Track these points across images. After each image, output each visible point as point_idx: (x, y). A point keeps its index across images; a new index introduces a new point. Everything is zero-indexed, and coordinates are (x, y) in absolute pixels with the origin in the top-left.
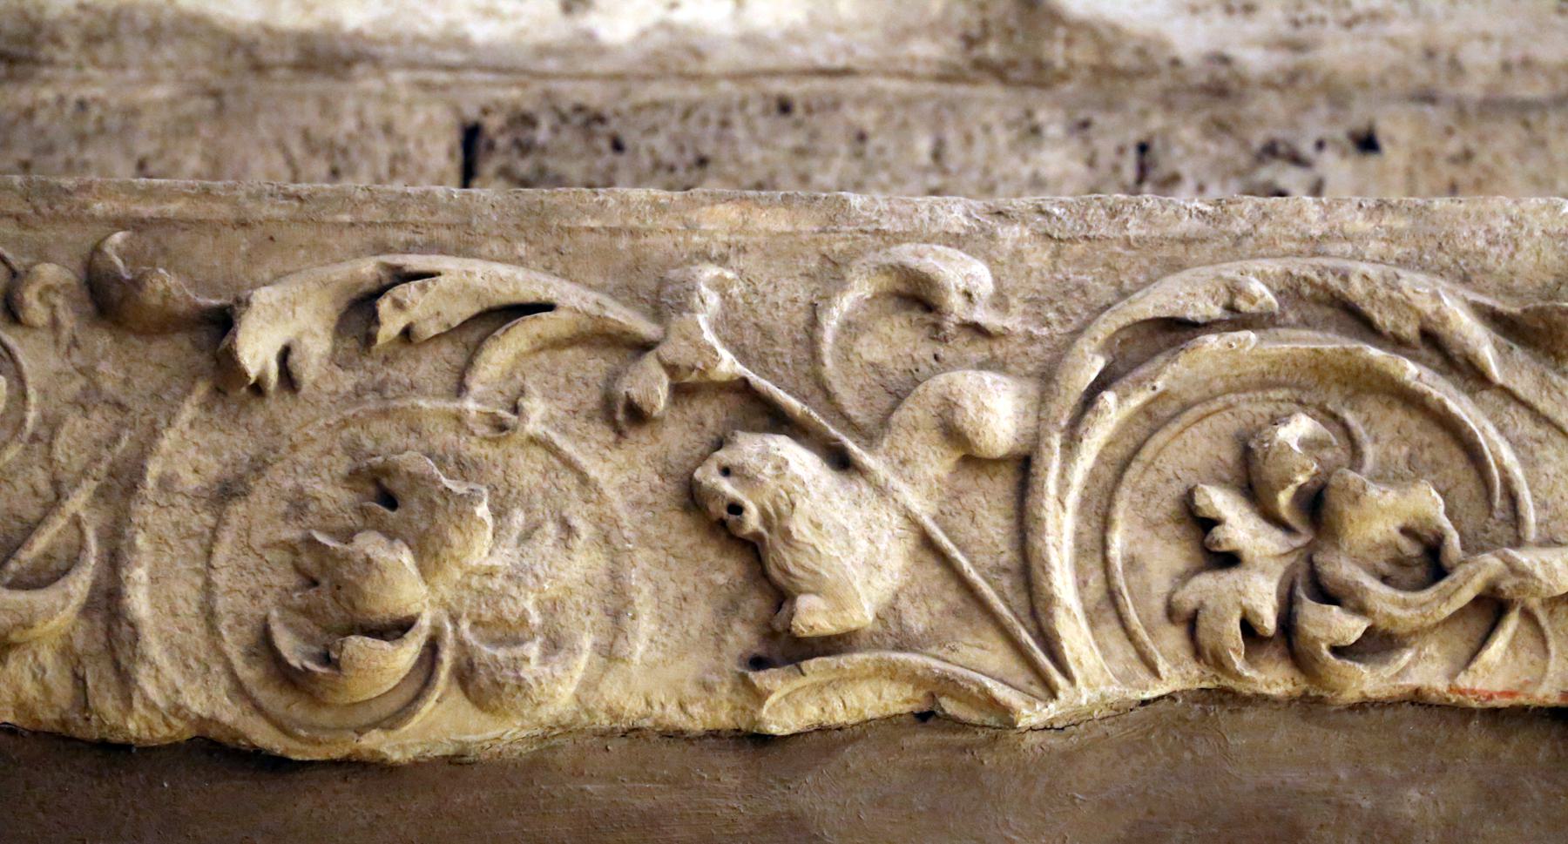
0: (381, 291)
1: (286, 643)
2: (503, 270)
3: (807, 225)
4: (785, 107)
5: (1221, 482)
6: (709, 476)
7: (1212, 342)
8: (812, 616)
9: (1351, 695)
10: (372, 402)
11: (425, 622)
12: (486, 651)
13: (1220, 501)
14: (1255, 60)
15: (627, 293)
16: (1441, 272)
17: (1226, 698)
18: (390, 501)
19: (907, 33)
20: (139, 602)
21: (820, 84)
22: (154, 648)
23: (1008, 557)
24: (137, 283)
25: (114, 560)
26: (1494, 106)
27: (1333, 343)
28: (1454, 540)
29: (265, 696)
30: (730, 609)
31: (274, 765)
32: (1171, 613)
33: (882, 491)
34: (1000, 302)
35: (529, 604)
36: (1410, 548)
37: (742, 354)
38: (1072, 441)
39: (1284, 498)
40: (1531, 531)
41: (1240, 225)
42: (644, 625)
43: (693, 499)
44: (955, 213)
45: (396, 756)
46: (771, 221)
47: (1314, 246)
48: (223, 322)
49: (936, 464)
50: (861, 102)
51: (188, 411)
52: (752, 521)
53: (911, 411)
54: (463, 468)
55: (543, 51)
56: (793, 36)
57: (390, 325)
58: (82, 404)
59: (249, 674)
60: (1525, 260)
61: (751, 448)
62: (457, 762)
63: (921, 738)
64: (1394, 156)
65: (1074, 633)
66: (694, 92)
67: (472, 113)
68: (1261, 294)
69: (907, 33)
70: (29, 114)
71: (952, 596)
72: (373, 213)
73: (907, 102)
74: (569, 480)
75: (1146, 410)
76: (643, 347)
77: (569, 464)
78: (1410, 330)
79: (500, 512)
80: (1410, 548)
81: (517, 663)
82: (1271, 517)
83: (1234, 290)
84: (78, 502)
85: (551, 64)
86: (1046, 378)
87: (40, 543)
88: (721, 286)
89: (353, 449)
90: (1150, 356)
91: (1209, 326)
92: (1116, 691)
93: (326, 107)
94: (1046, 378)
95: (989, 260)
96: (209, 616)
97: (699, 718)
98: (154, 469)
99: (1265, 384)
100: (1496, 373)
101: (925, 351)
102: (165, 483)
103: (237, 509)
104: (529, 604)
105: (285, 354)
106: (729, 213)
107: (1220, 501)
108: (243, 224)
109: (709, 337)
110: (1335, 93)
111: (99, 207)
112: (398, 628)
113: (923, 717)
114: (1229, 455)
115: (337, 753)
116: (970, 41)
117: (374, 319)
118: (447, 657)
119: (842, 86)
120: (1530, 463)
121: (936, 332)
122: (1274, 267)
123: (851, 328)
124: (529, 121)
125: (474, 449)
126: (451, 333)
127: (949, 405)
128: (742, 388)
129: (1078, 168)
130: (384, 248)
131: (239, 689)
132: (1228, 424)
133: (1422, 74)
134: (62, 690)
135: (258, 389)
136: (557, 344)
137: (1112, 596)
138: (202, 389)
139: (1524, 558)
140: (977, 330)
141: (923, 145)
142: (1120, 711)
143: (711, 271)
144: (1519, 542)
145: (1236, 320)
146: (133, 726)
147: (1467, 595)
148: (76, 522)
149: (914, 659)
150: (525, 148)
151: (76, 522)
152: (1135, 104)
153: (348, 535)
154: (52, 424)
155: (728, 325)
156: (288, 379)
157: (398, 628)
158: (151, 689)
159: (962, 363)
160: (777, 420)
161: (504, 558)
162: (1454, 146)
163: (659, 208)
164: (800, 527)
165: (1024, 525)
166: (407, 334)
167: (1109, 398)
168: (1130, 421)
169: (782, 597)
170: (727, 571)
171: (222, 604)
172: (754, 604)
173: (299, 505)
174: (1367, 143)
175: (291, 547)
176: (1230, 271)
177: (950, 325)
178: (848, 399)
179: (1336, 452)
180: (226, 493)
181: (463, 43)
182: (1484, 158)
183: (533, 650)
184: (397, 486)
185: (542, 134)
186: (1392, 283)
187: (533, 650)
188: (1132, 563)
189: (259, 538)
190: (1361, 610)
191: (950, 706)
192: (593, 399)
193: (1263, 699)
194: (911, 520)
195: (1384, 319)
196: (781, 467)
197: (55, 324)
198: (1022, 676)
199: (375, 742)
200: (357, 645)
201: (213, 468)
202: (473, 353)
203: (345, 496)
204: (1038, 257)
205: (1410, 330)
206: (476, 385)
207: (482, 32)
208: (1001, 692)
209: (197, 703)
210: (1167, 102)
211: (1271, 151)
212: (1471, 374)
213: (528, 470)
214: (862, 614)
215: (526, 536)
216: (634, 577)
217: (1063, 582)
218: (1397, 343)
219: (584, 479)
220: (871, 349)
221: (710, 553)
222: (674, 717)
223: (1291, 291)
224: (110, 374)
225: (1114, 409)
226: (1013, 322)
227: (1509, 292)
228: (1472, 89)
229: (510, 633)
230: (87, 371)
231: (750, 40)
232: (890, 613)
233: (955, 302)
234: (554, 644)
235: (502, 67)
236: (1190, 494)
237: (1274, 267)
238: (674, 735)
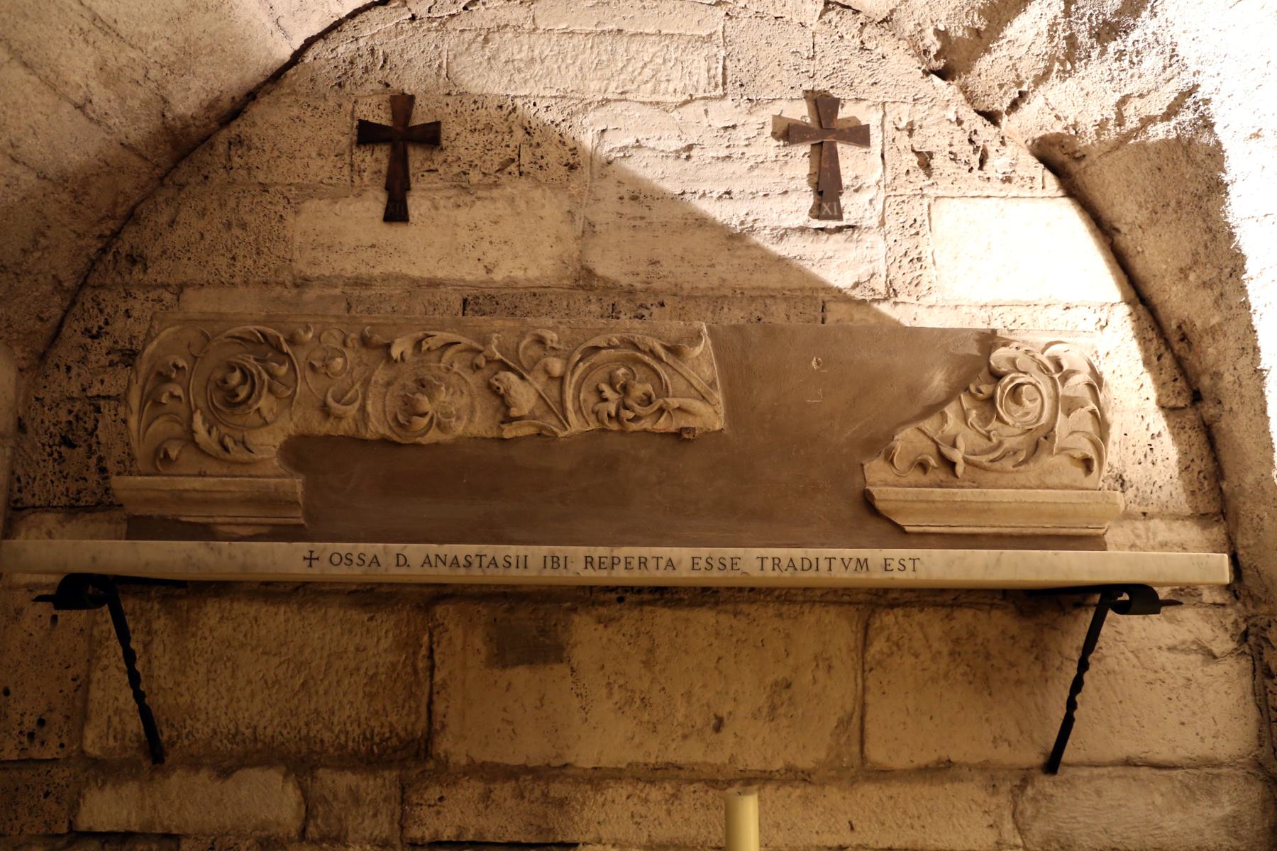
0: (422, 340)
1: (400, 418)
2: (450, 335)
3: (518, 325)
4: (535, 295)
5: (604, 382)
6: (493, 381)
7: (604, 352)
8: (514, 412)
9: (631, 430)
10: (421, 364)
11: (430, 414)
12: (443, 420)
13: (604, 387)
14: (639, 286)
15: (478, 340)
16: (655, 337)
17: (604, 430)
18: (423, 386)
19: (563, 278)
20: (370, 408)
21: (543, 290)
22: (373, 419)
23: (558, 399)
24: (371, 338)
25: (364, 399)
26: (690, 297)
27: (630, 352)
28: (654, 396)
29: (396, 429)
30: (497, 410)
31: (399, 445)
32: (593, 412)
33: (531, 384)
34: (559, 342)
35: (453, 409)
36: (644, 397)
37: (502, 354)
38: (573, 373)
39: (618, 387)
40: (671, 394)
41: (612, 326)
42: (478, 414)
43: (489, 386)
44: (550, 323)
45: (424, 443)
46: (510, 324)
47: (628, 331)
48: (388, 346)
49: (543, 378)
50: (551, 294)
51: (381, 366)
52: (502, 391)
53: (538, 367)
54: (440, 379)
55: (482, 282)
56: (537, 279)
57: (425, 347)
58: (359, 365)
59: (393, 424)
60: (673, 334)
61: (503, 375)
62: (437, 444)
63: (538, 439)
64: (667, 308)
65: (572, 417)
66: (515, 291)
67: (465, 296)
68: (615, 341)
69: (563, 278)
70: (369, 297)
71: (546, 408)
72: (423, 322)
73: (561, 294)
74: (463, 382)
75: (590, 366)
76: (480, 352)
77: (463, 378)
78: (647, 350)
79: (447, 389)
80: (644, 397)
81: (449, 422)
82: (616, 391)
83: (610, 340)
84: (357, 386)
85: (483, 285)
86: (568, 359)
87: (349, 395)
88: (498, 338)
89: (416, 374)
90: (590, 355)
91: (604, 348)
92: (580, 429)
93: (433, 295)
94: (568, 359)
95: (557, 333)
96: (384, 412)
97: (490, 435)
98: (373, 379)
99: (616, 361)
100: (665, 359)
101: (542, 353)
102: (376, 382)
103: (391, 388)
104: (453, 409)
105: (402, 353)
106: (500, 322)
107: (604, 387)
108: (395, 324)
109: (494, 350)
110: (656, 293)
111: (364, 321)
112: (424, 415)
113: (539, 434)
114: (607, 377)
115: (411, 442)
116: (576, 281)
117: (421, 346)
118: (435, 421)
119: (547, 290)
120: (671, 378)
121: (545, 349)
122: (618, 335)
123: (526, 348)
124: (478, 298)
125: (442, 374)
126: (438, 349)
127: (546, 365)
128: (501, 361)
129: (599, 309)
130: (425, 330)
131: (390, 428)
132: (607, 370)
133: (674, 289)
134: (353, 427)
135: (396, 361)
136: (461, 351)
137: (580, 408)
138: (384, 361)
139: (668, 400)
140: (553, 348)
141: (565, 304)
142: (582, 433)
143: (496, 335)
144: (668, 396)
145: (610, 347)
146: (368, 436)
147: (656, 408)
148: (357, 391)
149: (537, 422)
150: (477, 304)
151: (357, 391)
152: (612, 295)
153: (414, 394)
154: (352, 369)
155: (499, 348)
156: (403, 359)
157: (424, 415)
158: (372, 428)
159: (550, 356)
160: (509, 368)
161: (448, 399)
162: (680, 306)
163: (485, 321)
164: (512, 393)
165: (562, 392)
166: (429, 349)
167: (581, 364)
168: (585, 370)
169: (508, 408)
170: (497, 402)
171: (387, 409)
172: (503, 409)
173: (404, 386)
174: (662, 305)
175: (402, 396)
176: (609, 336)
177: (548, 347)
178: (525, 363)
179: (630, 376)
180: (389, 384)
181: (464, 280)
182: (687, 308)
183: (453, 420)
184: (425, 383)
185: (481, 301)
186: (644, 339)
187: (453, 420)
188: (585, 401)
189: (395, 394)
190: (633, 411)
191: (544, 432)
192: (469, 363)
193: (611, 431)
194: (537, 391)
195: (641, 347)
196: (508, 379)
197: (354, 347)
198: (560, 426)
199: (419, 439)
200: (415, 418)
201: (386, 379)
202: (443, 353)
203: (414, 385)
204: (568, 332)
205: (647, 350)
206: (443, 360)
207: (468, 278)
208: (555, 429)
209: (381, 431)
210: (619, 295)
211: (641, 306)
212: (659, 359)
213: (454, 379)
214: (525, 412)
215: (453, 394)
216: (476, 403)
217: (569, 405)
218: (644, 352)
219: (466, 382)
220: (530, 353)
221: (493, 398)
222: (484, 434)
223: (622, 340)
224: (365, 358)
225: (582, 366)
226: (561, 347)
227: (669, 341)
228: (685, 293)
229: (449, 416)
230: (360, 357)
231: (527, 280)
232: (532, 411)
233: (549, 342)
234: (459, 418)
235: (472, 286)
236: (597, 386)
237: (618, 335)
238: (484, 438)
